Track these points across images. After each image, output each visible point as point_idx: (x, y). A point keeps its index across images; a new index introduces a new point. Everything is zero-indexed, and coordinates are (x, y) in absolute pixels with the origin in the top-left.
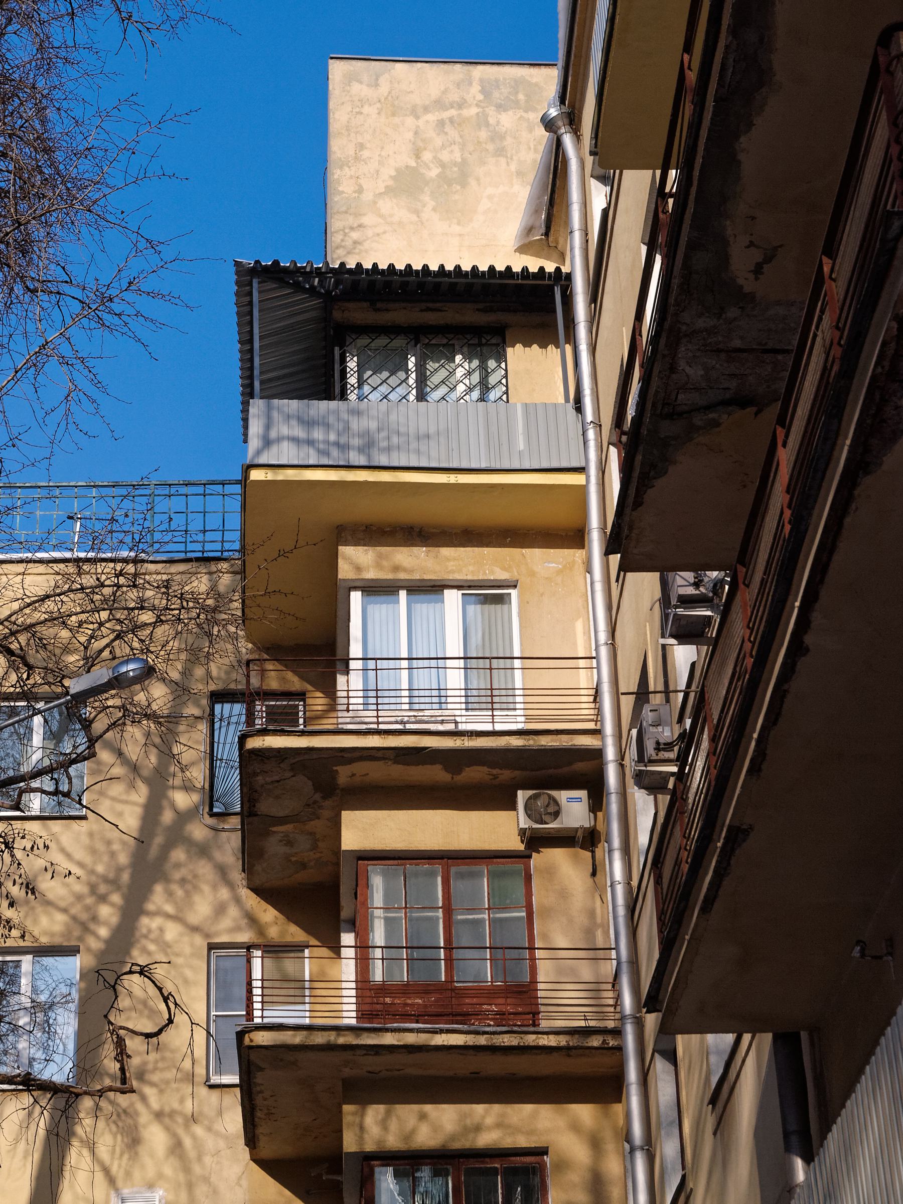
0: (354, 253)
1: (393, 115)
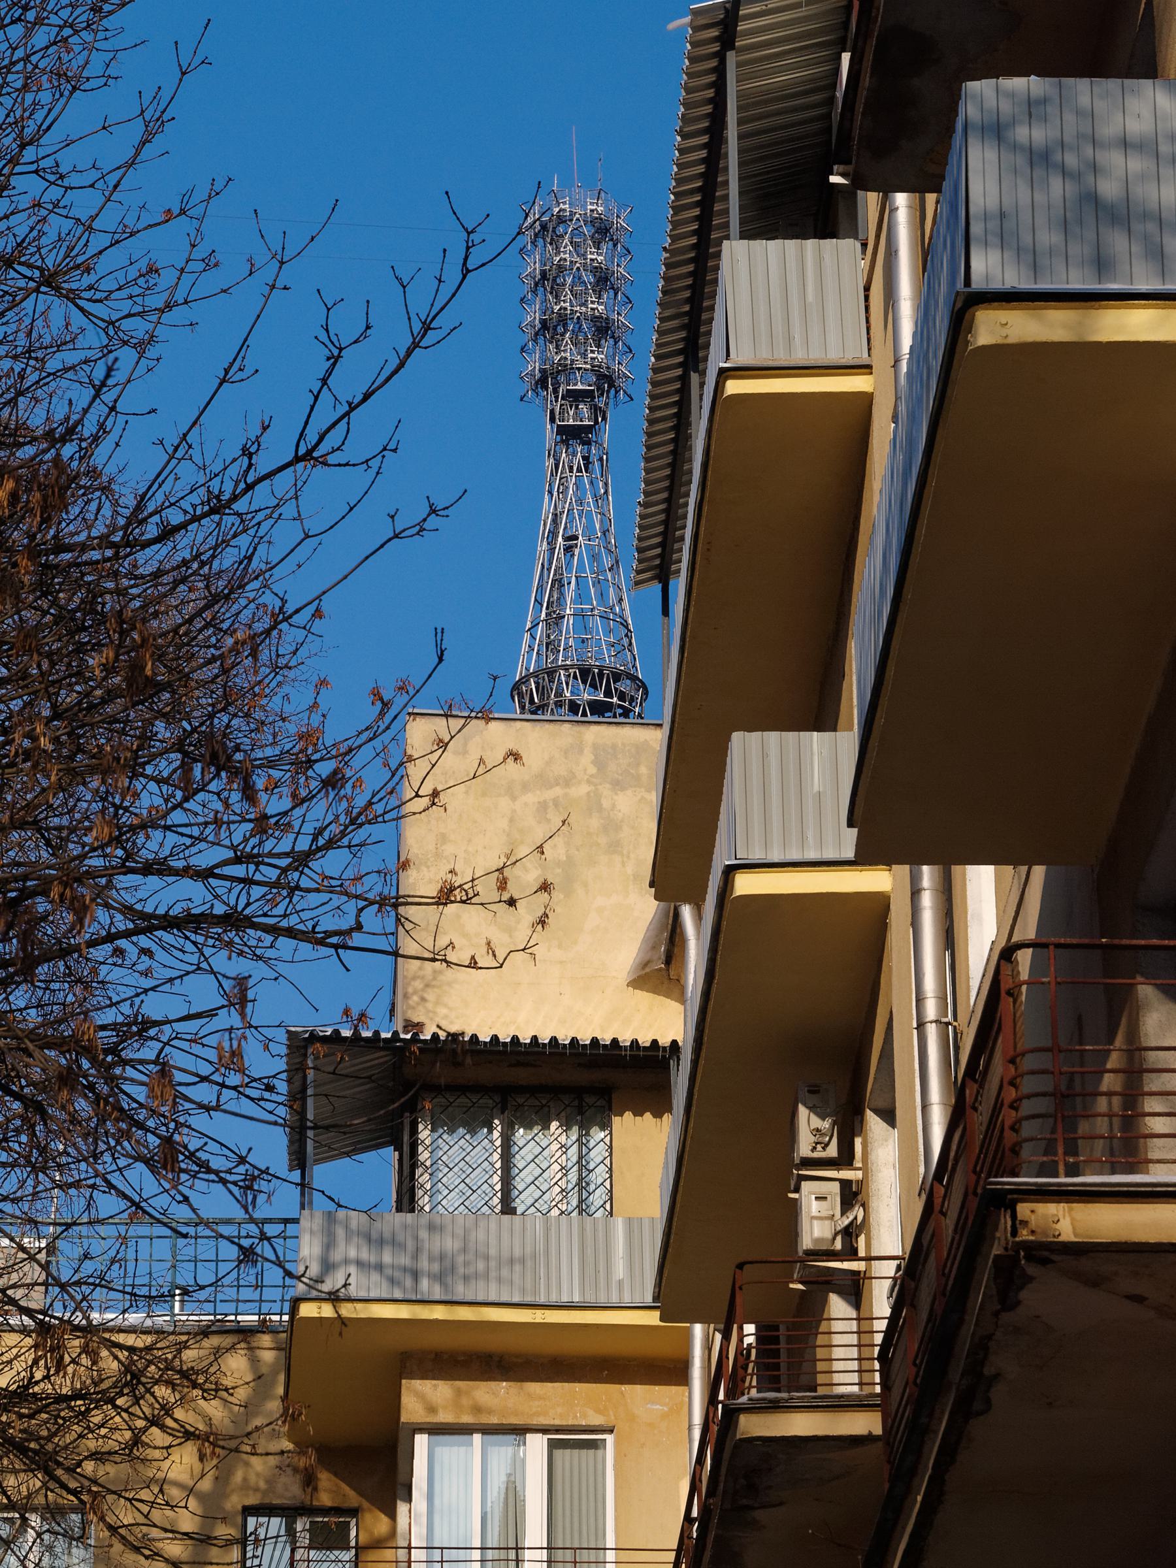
0: (434, 986)
1: (484, 794)
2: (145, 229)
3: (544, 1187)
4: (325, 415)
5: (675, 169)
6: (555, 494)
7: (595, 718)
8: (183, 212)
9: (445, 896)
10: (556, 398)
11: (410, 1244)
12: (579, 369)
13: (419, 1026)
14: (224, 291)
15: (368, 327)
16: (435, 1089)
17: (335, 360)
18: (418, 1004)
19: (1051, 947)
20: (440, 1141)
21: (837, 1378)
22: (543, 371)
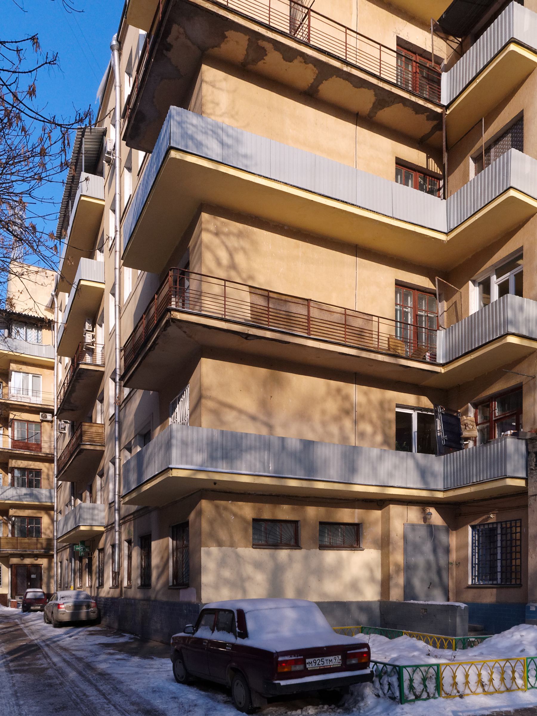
16: (15, 320)
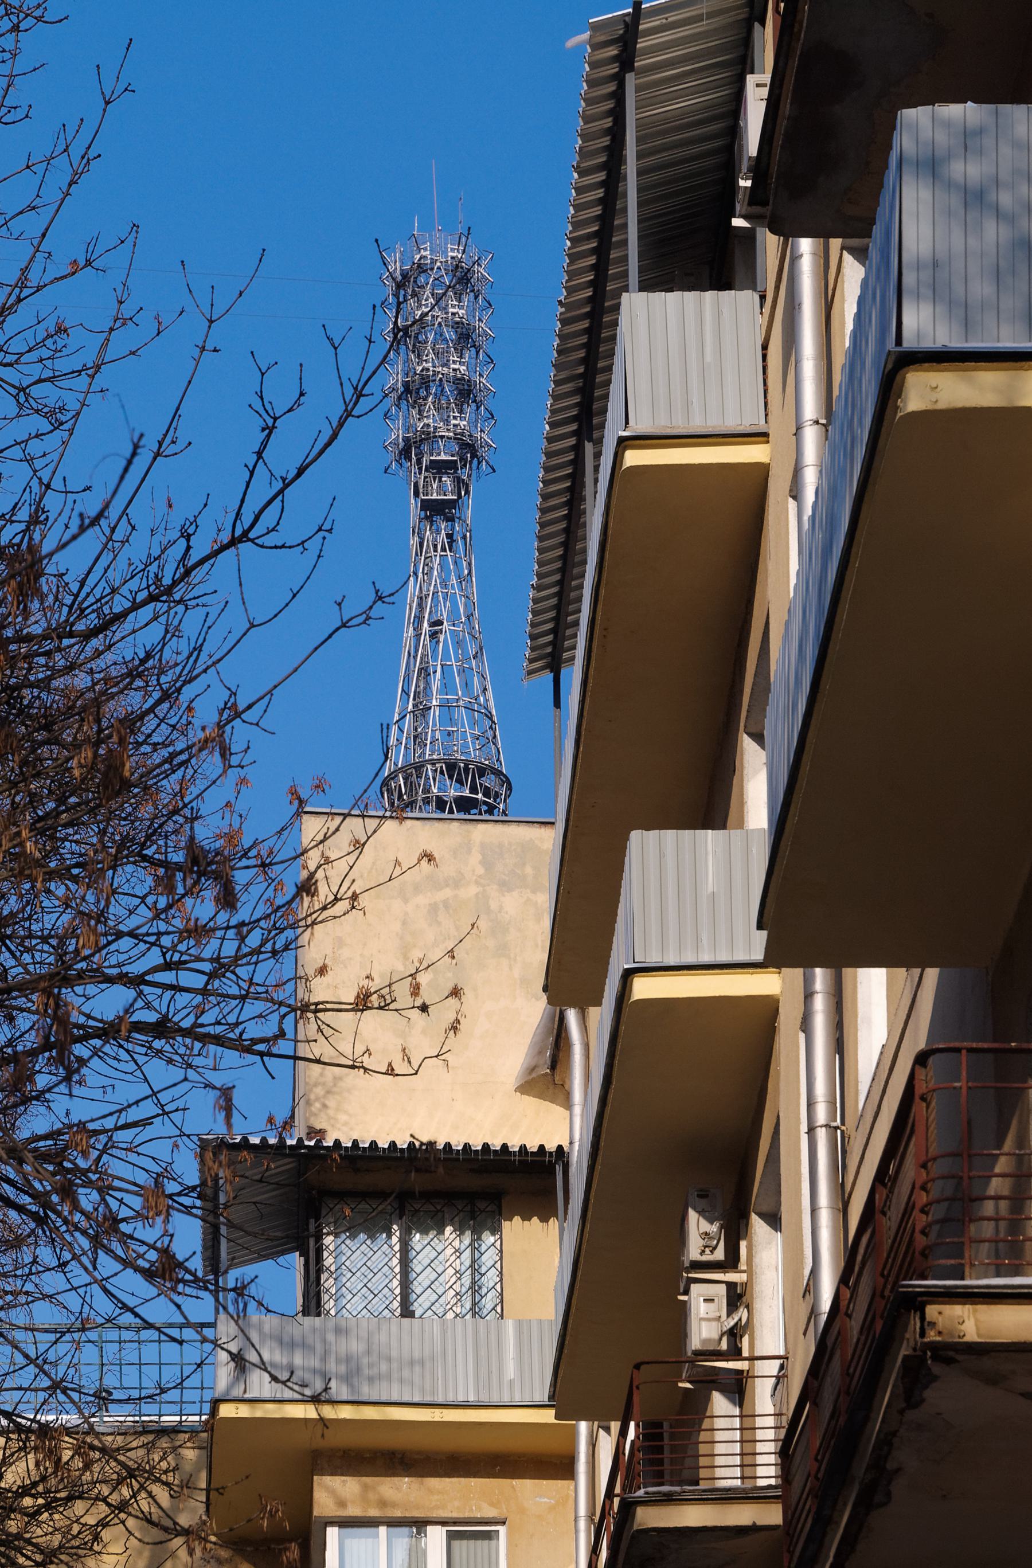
2: (52, 282)
3: (440, 1292)
4: (261, 490)
5: (572, 211)
6: (420, 575)
7: (462, 816)
8: (89, 263)
9: (362, 1003)
10: (420, 469)
11: (319, 1347)
12: (442, 437)
13: (322, 1132)
14: (133, 353)
15: (302, 394)
16: (342, 1195)
17: (269, 430)
18: (320, 1110)
19: (964, 1052)
20: (343, 1246)
21: (719, 1472)
22: (406, 440)
